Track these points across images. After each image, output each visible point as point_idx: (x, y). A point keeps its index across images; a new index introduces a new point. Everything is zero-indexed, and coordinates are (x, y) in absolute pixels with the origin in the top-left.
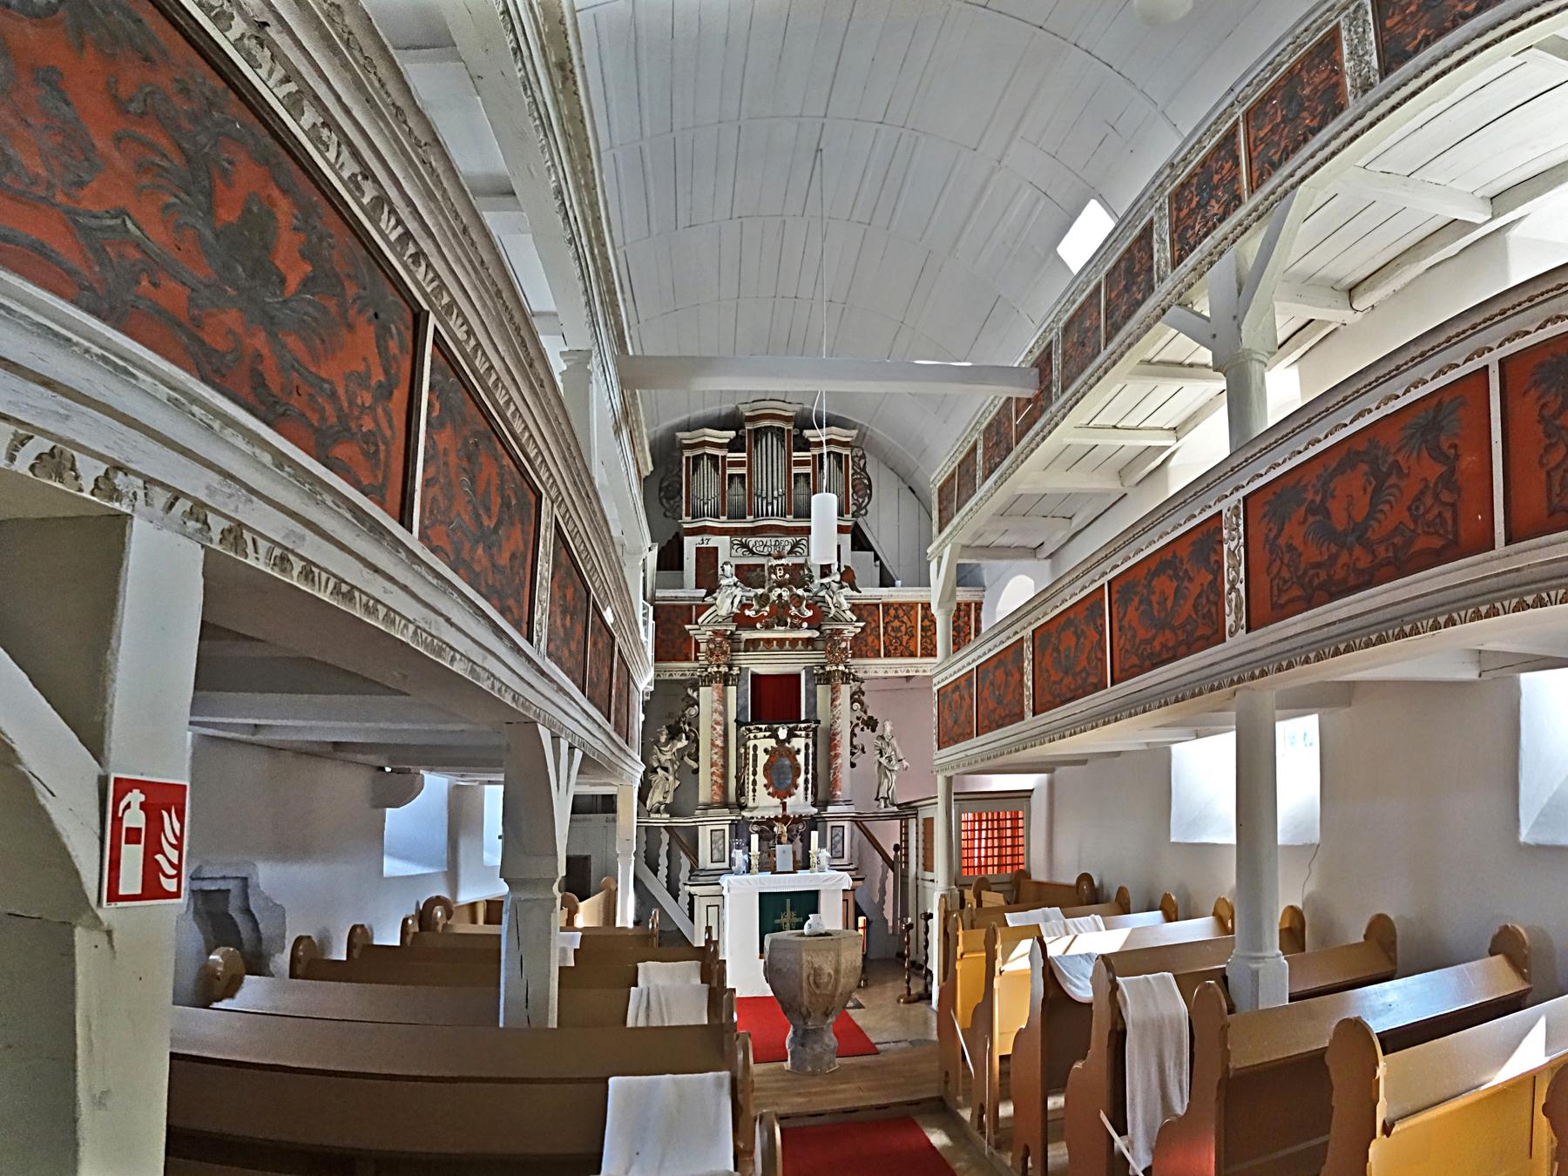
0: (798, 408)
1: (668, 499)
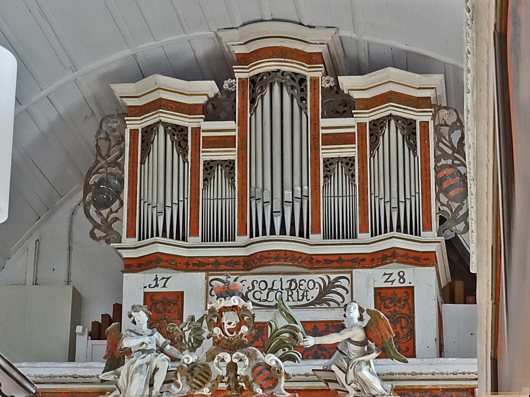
0: (327, 36)
1: (99, 206)
